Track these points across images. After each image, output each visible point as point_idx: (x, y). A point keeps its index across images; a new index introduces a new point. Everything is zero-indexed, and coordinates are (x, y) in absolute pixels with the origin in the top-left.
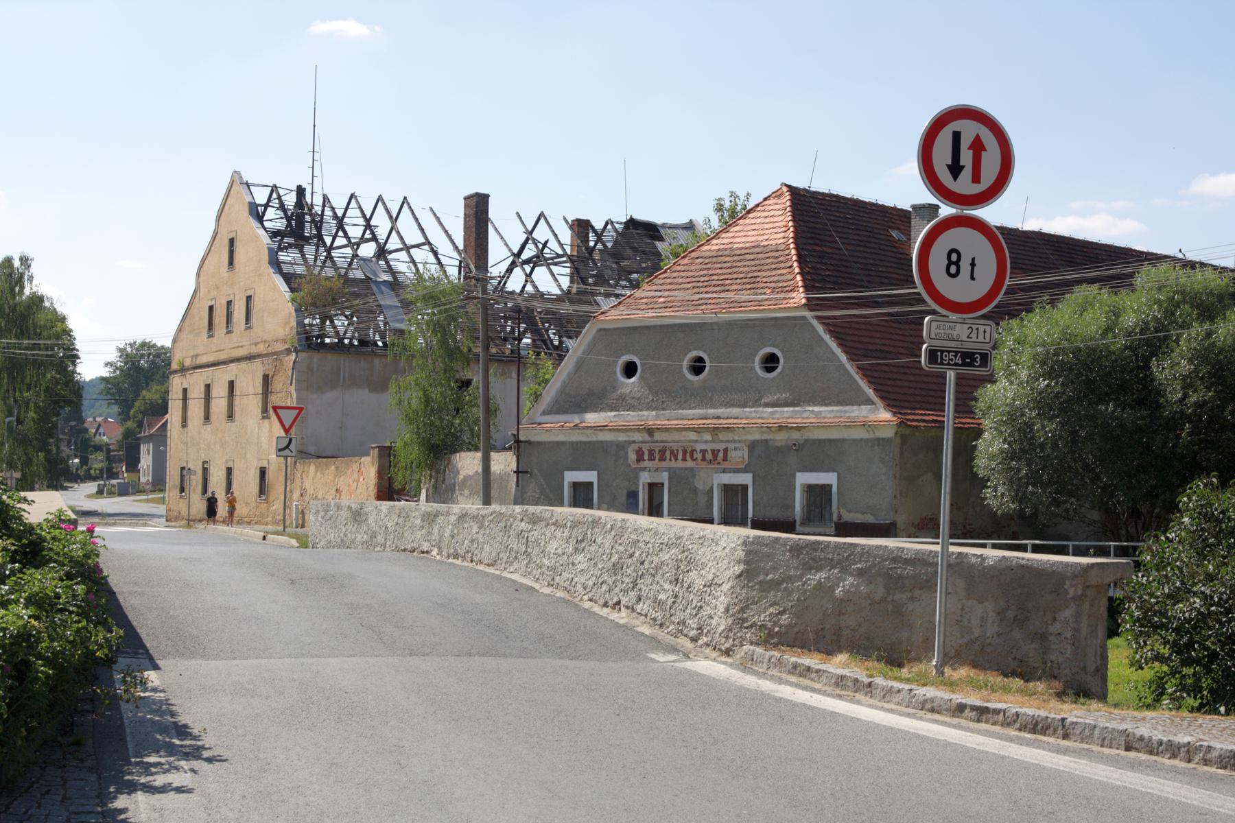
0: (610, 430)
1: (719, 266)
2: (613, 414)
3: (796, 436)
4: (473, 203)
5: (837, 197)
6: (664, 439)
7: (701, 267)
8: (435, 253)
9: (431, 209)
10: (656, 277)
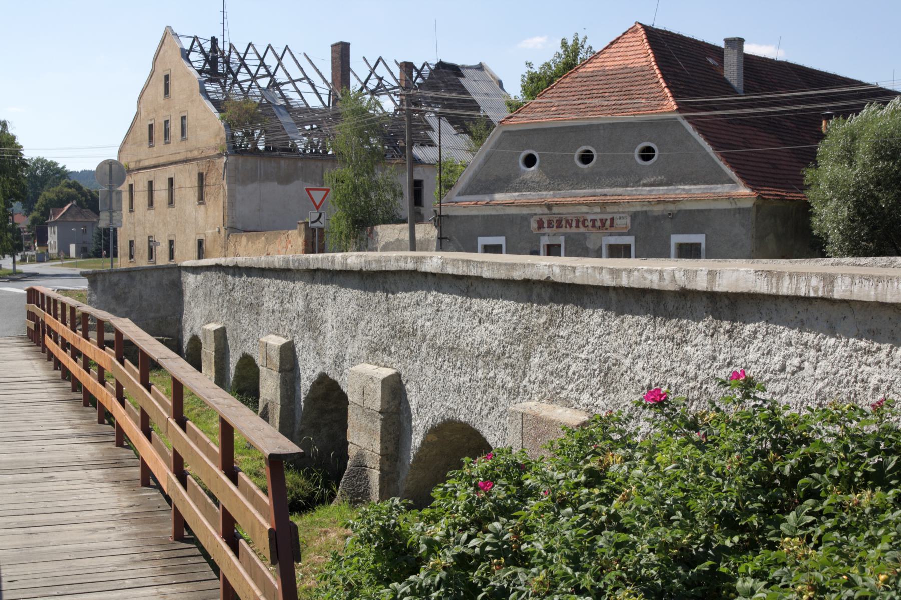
0: (516, 206)
1: (596, 83)
2: (517, 194)
3: (671, 208)
4: (339, 49)
5: (670, 33)
6: (561, 212)
7: (580, 84)
8: (313, 86)
9: (305, 55)
10: (545, 92)
